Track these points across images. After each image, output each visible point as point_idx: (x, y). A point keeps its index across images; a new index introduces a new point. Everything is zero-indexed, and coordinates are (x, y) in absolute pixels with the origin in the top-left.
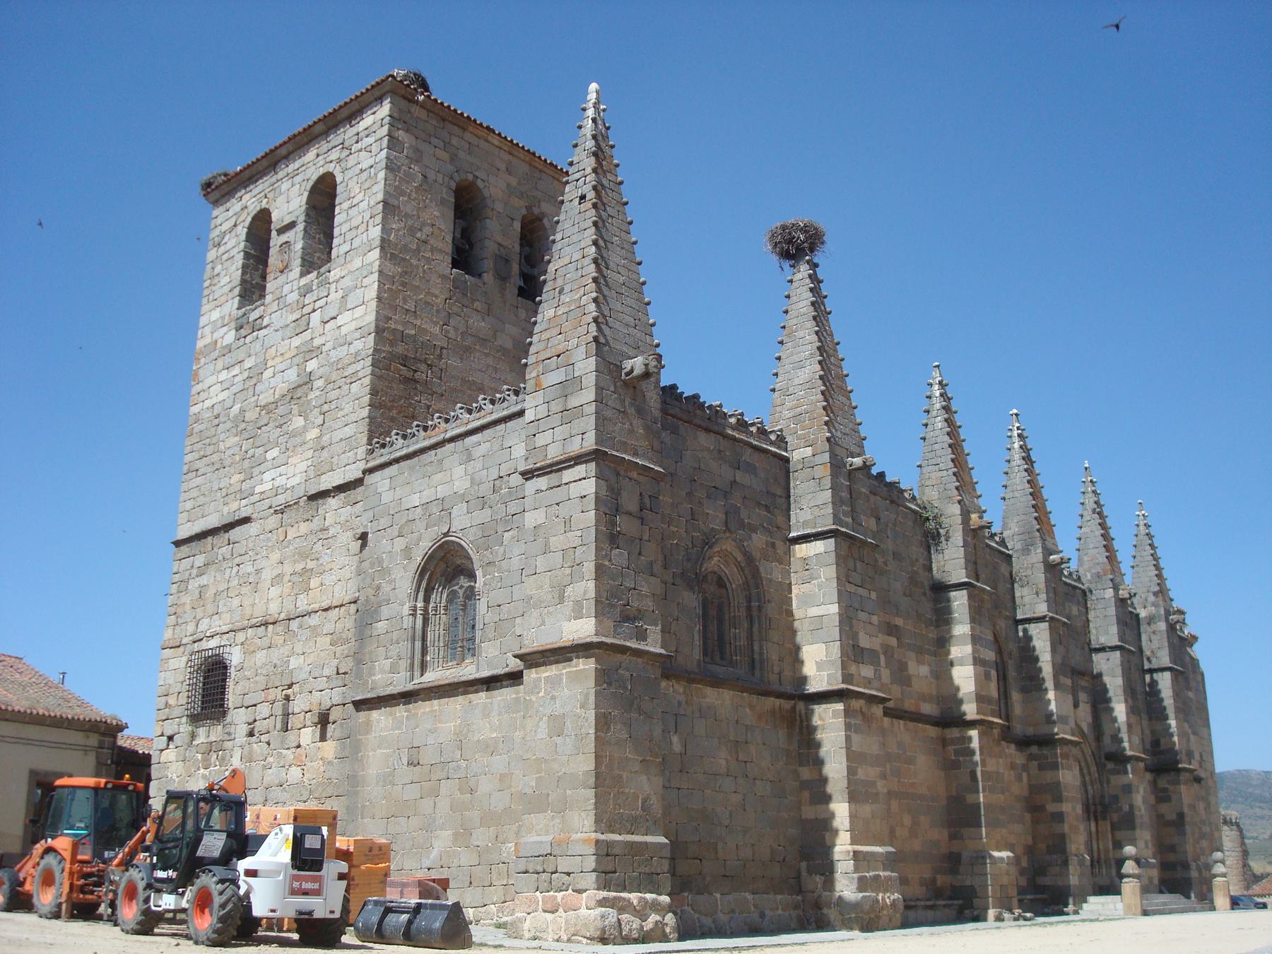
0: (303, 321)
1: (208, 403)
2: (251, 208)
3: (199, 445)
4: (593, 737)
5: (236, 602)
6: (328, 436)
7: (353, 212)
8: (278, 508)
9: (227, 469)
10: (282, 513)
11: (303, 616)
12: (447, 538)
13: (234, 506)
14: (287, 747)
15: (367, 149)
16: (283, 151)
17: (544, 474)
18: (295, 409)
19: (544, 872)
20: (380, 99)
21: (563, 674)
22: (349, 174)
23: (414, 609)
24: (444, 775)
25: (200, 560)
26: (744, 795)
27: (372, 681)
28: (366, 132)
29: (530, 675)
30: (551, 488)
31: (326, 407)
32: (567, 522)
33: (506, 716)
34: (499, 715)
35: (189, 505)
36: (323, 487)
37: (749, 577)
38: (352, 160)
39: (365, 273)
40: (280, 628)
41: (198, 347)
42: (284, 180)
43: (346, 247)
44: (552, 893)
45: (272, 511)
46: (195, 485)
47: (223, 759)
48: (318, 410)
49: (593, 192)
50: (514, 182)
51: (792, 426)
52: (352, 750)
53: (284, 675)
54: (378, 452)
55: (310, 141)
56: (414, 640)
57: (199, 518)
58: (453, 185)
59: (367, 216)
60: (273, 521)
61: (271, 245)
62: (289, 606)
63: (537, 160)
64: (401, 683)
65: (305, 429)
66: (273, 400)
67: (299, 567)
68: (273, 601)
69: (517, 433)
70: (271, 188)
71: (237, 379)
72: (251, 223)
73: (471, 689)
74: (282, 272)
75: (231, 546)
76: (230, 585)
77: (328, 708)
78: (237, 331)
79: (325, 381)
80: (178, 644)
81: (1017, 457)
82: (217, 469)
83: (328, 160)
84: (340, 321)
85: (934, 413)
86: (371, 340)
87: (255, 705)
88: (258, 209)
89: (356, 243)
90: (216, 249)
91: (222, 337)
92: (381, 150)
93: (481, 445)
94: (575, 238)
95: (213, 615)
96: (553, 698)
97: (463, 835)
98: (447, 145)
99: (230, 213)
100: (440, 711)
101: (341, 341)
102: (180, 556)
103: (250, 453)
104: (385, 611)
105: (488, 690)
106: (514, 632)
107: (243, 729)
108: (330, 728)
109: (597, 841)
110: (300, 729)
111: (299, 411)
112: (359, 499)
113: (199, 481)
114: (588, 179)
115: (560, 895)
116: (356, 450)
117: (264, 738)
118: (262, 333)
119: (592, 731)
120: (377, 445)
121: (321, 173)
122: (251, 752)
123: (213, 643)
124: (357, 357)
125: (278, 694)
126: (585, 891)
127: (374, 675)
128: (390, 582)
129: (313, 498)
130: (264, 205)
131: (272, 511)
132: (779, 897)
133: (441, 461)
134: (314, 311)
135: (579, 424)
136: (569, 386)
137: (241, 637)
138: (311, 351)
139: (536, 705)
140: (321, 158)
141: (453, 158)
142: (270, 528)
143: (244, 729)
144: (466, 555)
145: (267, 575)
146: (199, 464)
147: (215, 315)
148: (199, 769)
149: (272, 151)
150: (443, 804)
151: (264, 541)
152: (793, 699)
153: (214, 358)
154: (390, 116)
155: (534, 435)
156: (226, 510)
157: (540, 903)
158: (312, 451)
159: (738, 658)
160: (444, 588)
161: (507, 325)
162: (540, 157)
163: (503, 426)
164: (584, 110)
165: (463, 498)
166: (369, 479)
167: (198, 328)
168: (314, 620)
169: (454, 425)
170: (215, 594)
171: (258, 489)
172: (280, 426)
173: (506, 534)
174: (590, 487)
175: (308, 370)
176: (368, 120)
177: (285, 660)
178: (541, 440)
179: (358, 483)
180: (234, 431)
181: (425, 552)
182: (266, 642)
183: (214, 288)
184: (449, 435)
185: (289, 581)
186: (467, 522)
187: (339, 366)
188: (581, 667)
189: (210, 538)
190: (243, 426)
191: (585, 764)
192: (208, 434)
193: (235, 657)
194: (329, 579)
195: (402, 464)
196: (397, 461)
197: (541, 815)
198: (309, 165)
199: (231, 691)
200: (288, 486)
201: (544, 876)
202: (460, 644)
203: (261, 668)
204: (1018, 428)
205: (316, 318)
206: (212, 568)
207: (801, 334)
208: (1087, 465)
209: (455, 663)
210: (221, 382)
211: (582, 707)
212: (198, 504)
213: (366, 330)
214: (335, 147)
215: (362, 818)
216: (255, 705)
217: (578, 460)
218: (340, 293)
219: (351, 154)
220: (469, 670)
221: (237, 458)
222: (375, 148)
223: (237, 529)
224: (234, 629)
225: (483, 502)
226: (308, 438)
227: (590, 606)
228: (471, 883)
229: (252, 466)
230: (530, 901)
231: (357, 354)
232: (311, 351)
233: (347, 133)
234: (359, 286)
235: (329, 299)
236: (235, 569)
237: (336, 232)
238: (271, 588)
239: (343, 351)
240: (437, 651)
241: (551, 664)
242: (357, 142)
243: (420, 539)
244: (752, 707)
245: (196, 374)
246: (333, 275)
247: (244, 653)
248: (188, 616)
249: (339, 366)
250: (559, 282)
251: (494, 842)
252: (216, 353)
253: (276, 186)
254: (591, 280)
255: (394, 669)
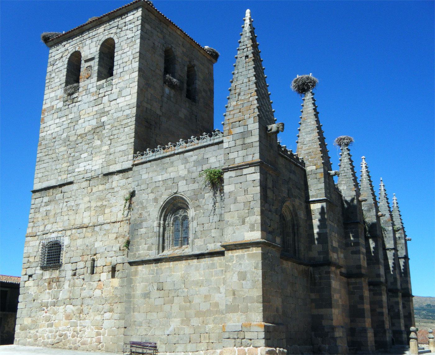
0: (99, 100)
1: (49, 132)
2: (70, 50)
3: (45, 150)
4: (261, 281)
5: (66, 218)
6: (113, 149)
7: (123, 56)
8: (88, 179)
9: (60, 161)
10: (90, 181)
11: (102, 225)
12: (176, 195)
13: (64, 177)
14: (93, 281)
15: (131, 30)
16: (87, 27)
17: (233, 170)
18: (96, 137)
19: (238, 338)
20: (137, 9)
21: (245, 254)
22: (121, 39)
23: (160, 224)
24: (176, 294)
25: (46, 199)
26: (295, 305)
27: (138, 254)
28: (130, 22)
29: (228, 254)
30: (237, 176)
31: (112, 137)
32: (246, 191)
33: (207, 270)
34: (204, 270)
35: (40, 175)
36: (111, 171)
37: (294, 216)
38: (123, 34)
39: (131, 82)
40: (89, 230)
41: (43, 108)
42: (87, 39)
43: (121, 70)
44: (242, 348)
45: (84, 179)
46: (42, 167)
47: (59, 286)
48: (108, 138)
49: (252, 54)
50: (185, 50)
51: (306, 157)
52: (129, 281)
53: (92, 250)
54: (139, 158)
55: (101, 24)
56: (159, 237)
57: (45, 181)
58: (164, 49)
59: (131, 58)
60: (85, 184)
61: (81, 67)
62: (94, 220)
63: (193, 42)
64: (153, 254)
65: (101, 146)
66: (84, 133)
67: (99, 204)
68: (86, 218)
69: (211, 153)
70: (81, 42)
71: (64, 123)
72: (70, 57)
73: (190, 258)
74: (87, 78)
75: (63, 194)
76: (63, 210)
77: (115, 264)
78: (64, 102)
79: (111, 126)
80: (35, 235)
81: (365, 175)
82: (55, 161)
83: (111, 32)
84: (118, 101)
85: (344, 156)
86: (134, 110)
87: (76, 262)
88: (74, 51)
89: (126, 69)
90: (52, 66)
91: (57, 105)
92: (138, 30)
93: (193, 157)
94: (244, 73)
95: (53, 223)
96: (240, 264)
97: (186, 320)
98: (162, 32)
99: (59, 52)
100: (174, 267)
101: (119, 110)
102: (35, 197)
103: (72, 155)
104: (144, 224)
105: (198, 259)
106: (211, 235)
107: (70, 273)
108: (117, 273)
109: (265, 326)
110: (100, 273)
111: (98, 138)
112: (130, 176)
113: (45, 165)
114: (249, 49)
115: (246, 349)
116: (128, 156)
117: (81, 277)
118: (77, 104)
119: (261, 279)
120: (139, 154)
121: (107, 38)
122: (74, 283)
123: (54, 235)
124: (127, 117)
125: (89, 258)
126: (259, 347)
127: (139, 251)
128: (147, 212)
129: (106, 175)
130: (77, 49)
131: (84, 179)
132: (306, 346)
133: (172, 163)
134: (105, 96)
135: (250, 151)
136: (244, 135)
137: (69, 233)
138: (104, 113)
139: (232, 267)
140: (106, 32)
141: (164, 38)
142: (83, 187)
143: (71, 273)
144: (184, 202)
145: (82, 207)
146: (44, 158)
147: (52, 95)
148: (46, 290)
149: (81, 26)
150: (175, 308)
151: (80, 192)
152: (308, 266)
153: (52, 113)
154: (141, 16)
155: (228, 154)
156: (60, 178)
157: (237, 352)
158: (105, 155)
159: (290, 249)
160: (172, 215)
161: (182, 109)
162: (194, 41)
163: (204, 149)
164: (245, 20)
165: (184, 178)
166: (135, 168)
167: (43, 100)
168: (106, 227)
169: (179, 148)
170: (55, 214)
171: (77, 170)
172: (88, 144)
173: (206, 194)
174: (257, 176)
175: (102, 121)
176: (130, 17)
177: (93, 243)
178: (231, 156)
179: (130, 169)
180: (64, 145)
181: (165, 200)
182: (82, 235)
183: (51, 83)
184: (176, 152)
185: (94, 210)
186: (186, 188)
187: (117, 119)
188: (254, 252)
189: (51, 190)
190: (68, 143)
191: (258, 292)
192: (50, 145)
193: (66, 241)
194: (114, 210)
195: (153, 162)
196: (150, 161)
197: (235, 314)
198: (100, 34)
199: (64, 256)
200: (93, 169)
201: (238, 340)
202: (180, 239)
203: (80, 246)
204: (365, 164)
205: (105, 99)
206: (53, 203)
207: (309, 121)
208: (381, 179)
209: (178, 247)
210: (56, 124)
211: (255, 268)
212: (45, 175)
213: (132, 106)
214: (114, 27)
215: (133, 312)
216: (76, 262)
217: (251, 165)
218: (118, 90)
219: (122, 31)
220: (187, 250)
221: (66, 156)
222: (135, 29)
223: (66, 186)
224: (65, 229)
225: (194, 180)
226: (103, 150)
227: (258, 226)
228: (190, 341)
229: (73, 161)
230: (231, 351)
231: (127, 115)
232: (104, 113)
233: (119, 22)
234: (128, 87)
235: (112, 91)
236: (65, 204)
237: (115, 63)
238: (85, 213)
239: (120, 114)
240: (169, 242)
241: (238, 249)
242: (125, 26)
243: (162, 195)
244: (297, 269)
245: (43, 119)
246: (114, 82)
247: (71, 240)
248: (40, 223)
249: (119, 120)
250: (238, 91)
251: (202, 324)
252: (53, 111)
253: (83, 41)
254: (254, 91)
255: (149, 249)
